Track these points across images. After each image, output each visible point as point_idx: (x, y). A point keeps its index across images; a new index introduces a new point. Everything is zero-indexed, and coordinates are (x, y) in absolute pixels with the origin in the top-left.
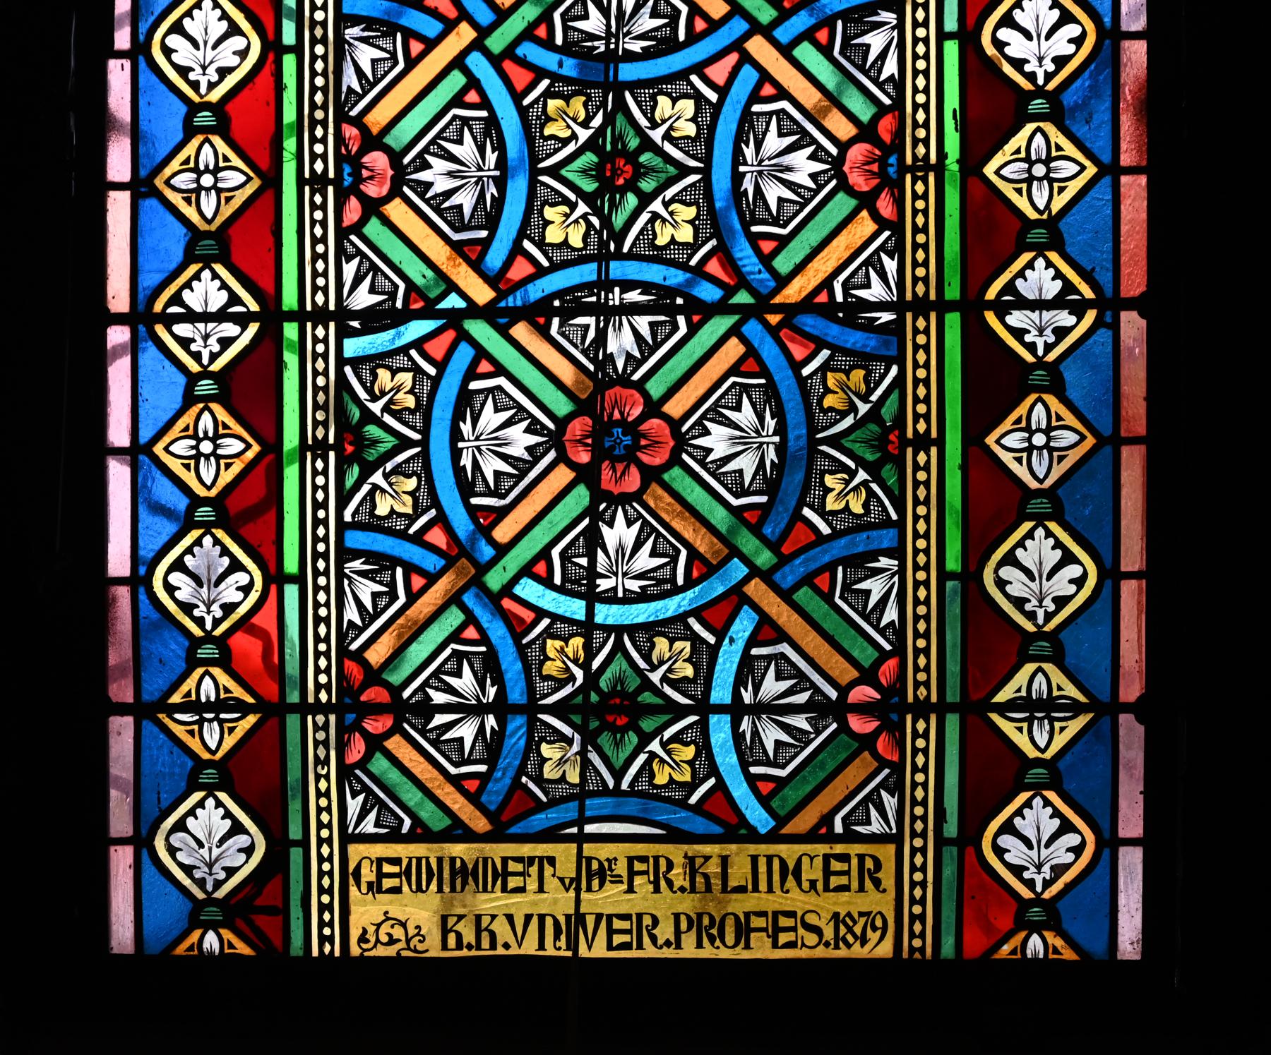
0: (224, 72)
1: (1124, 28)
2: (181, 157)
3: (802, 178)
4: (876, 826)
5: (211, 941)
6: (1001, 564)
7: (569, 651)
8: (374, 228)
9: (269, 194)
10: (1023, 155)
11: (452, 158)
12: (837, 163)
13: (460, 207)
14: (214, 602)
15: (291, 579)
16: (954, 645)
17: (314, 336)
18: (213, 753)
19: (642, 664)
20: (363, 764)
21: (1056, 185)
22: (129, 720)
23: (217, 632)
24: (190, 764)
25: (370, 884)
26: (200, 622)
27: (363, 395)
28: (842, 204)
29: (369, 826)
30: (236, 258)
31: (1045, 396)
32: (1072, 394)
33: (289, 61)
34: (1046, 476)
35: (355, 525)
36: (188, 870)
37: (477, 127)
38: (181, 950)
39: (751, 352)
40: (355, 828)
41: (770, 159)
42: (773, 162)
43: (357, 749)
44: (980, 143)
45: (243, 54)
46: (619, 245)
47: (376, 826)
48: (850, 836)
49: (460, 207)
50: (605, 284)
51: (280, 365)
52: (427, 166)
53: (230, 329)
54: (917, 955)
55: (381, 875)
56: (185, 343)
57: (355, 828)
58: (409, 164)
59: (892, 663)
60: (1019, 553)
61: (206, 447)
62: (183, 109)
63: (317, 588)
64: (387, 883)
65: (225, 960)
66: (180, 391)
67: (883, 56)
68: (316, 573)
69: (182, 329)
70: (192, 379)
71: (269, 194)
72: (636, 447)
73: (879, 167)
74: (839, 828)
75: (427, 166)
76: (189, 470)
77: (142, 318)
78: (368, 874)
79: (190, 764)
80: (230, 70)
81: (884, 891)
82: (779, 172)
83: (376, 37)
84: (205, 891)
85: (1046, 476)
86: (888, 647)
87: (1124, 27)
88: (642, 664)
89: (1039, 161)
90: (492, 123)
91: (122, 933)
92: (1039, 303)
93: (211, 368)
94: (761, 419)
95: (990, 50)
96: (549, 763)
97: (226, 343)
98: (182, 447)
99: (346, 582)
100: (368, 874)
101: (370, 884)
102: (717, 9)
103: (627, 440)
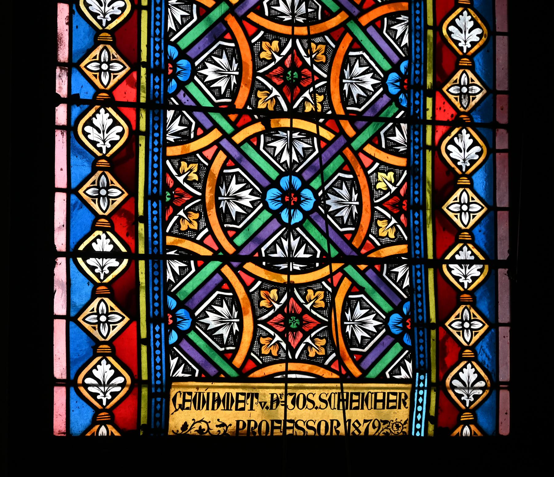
0: (114, 17)
1: (498, 205)
2: (91, 181)
3: (368, 86)
4: (404, 375)
5: (103, 431)
6: (449, 25)
7: (271, 296)
8: (181, 95)
9: (134, 324)
10: (458, 201)
11: (216, 64)
12: (385, 322)
13: (222, 335)
14: (107, 391)
15: (144, 8)
16: (430, 58)
17: (154, 81)
18: (105, 338)
19: (302, 301)
20: (177, 344)
21: (472, 215)
22: (64, 389)
23: (108, 407)
24: (93, 158)
25: (180, 405)
26: (100, 402)
27: (174, 173)
28: (388, 340)
29: (179, 373)
30: (116, 230)
31: (466, 70)
32: (478, 71)
33: (144, 14)
34: (467, 106)
35: (171, 234)
36: (95, 15)
37: (230, 50)
38: (88, 434)
39: (347, 162)
40: (173, 374)
41: (355, 77)
42: (357, 78)
43: (174, 337)
44: (444, 313)
45: (123, 9)
46: (293, 355)
47: (182, 373)
48: (393, 380)
49: (222, 335)
50: (287, 372)
51: (138, 145)
52: (205, 67)
53: (113, 262)
54: (418, 257)
55: (184, 400)
56: (92, 268)
57: (173, 374)
58: (199, 65)
59: (408, 304)
60: (457, 20)
61: (105, 67)
62: (92, 217)
63: (156, 12)
64: (187, 404)
65: (110, 437)
66: (89, 223)
67: (402, 35)
68: (154, 131)
69: (92, 261)
70: (97, 411)
71: (134, 324)
72: (299, 202)
73: (400, 84)
74: (388, 376)
75: (205, 67)
76: (95, 329)
77: (71, 254)
78: (179, 401)
79: (93, 158)
80: (117, 142)
81: (407, 408)
82: (359, 83)
83: (183, 5)
84: (102, 26)
85: (467, 106)
86: (405, 297)
87: (498, 89)
88: (302, 301)
89: (464, 86)
90: (235, 297)
91: (59, 424)
92: (464, 208)
93: (107, 28)
94: (353, 332)
95: (445, 32)
96: (260, 101)
97: (112, 269)
98: (92, 319)
99: (169, 10)
100: (179, 401)
101: (180, 405)
102: (334, 7)
103: (295, 199)
